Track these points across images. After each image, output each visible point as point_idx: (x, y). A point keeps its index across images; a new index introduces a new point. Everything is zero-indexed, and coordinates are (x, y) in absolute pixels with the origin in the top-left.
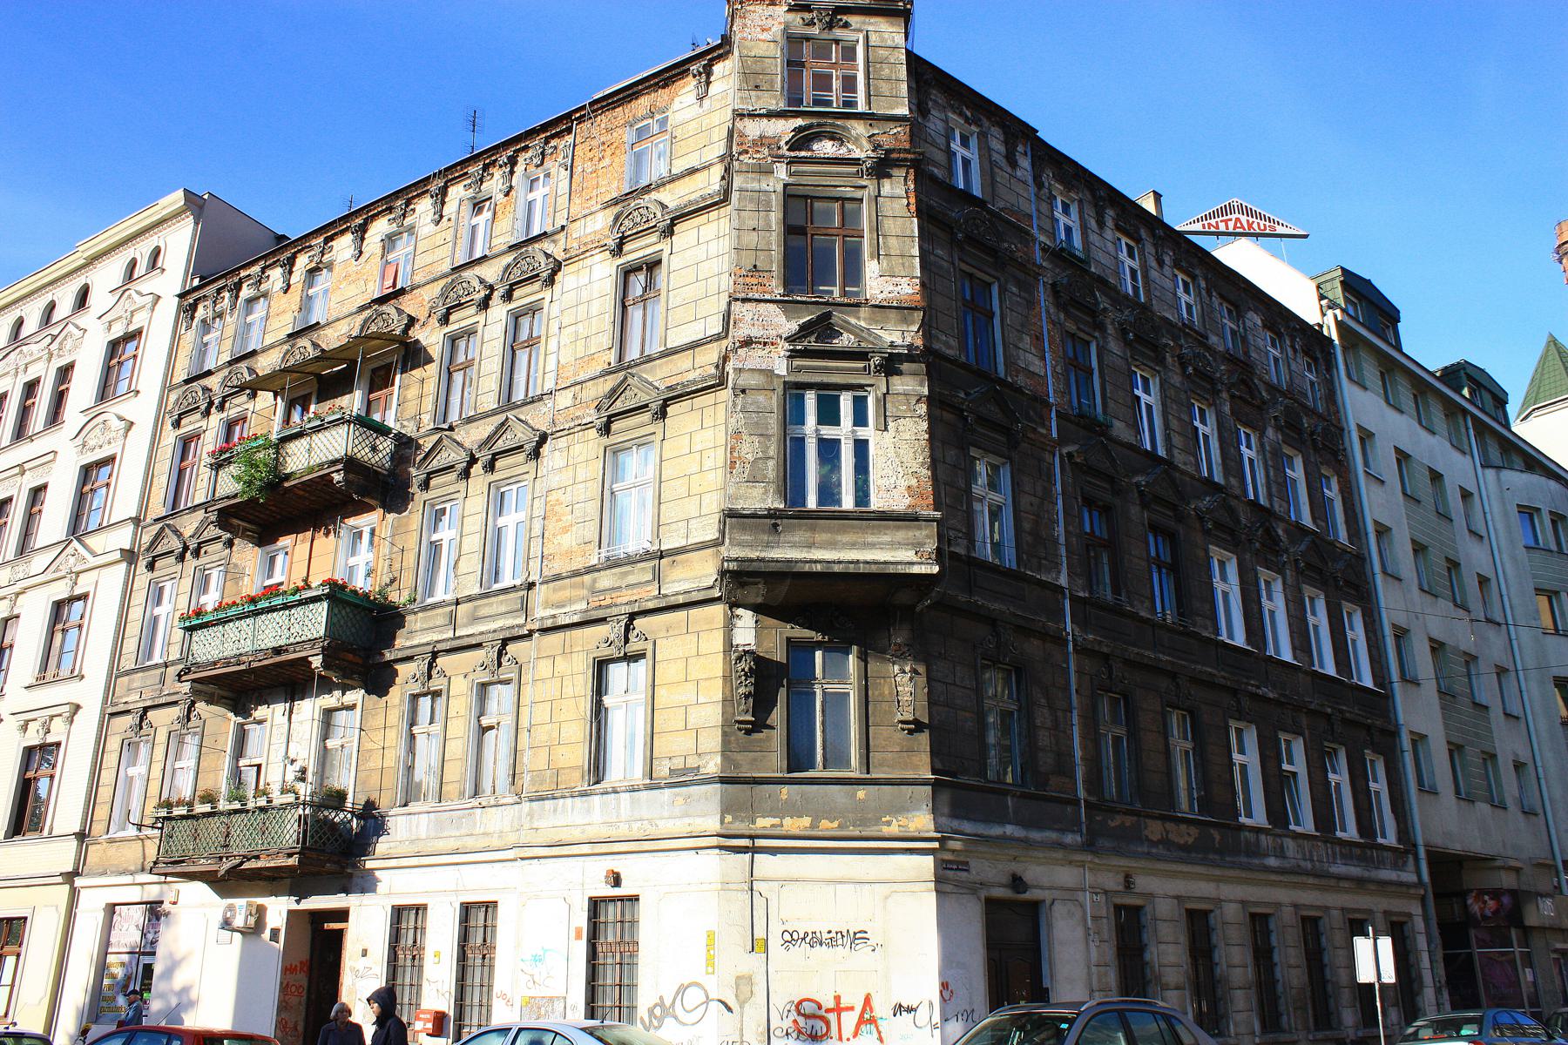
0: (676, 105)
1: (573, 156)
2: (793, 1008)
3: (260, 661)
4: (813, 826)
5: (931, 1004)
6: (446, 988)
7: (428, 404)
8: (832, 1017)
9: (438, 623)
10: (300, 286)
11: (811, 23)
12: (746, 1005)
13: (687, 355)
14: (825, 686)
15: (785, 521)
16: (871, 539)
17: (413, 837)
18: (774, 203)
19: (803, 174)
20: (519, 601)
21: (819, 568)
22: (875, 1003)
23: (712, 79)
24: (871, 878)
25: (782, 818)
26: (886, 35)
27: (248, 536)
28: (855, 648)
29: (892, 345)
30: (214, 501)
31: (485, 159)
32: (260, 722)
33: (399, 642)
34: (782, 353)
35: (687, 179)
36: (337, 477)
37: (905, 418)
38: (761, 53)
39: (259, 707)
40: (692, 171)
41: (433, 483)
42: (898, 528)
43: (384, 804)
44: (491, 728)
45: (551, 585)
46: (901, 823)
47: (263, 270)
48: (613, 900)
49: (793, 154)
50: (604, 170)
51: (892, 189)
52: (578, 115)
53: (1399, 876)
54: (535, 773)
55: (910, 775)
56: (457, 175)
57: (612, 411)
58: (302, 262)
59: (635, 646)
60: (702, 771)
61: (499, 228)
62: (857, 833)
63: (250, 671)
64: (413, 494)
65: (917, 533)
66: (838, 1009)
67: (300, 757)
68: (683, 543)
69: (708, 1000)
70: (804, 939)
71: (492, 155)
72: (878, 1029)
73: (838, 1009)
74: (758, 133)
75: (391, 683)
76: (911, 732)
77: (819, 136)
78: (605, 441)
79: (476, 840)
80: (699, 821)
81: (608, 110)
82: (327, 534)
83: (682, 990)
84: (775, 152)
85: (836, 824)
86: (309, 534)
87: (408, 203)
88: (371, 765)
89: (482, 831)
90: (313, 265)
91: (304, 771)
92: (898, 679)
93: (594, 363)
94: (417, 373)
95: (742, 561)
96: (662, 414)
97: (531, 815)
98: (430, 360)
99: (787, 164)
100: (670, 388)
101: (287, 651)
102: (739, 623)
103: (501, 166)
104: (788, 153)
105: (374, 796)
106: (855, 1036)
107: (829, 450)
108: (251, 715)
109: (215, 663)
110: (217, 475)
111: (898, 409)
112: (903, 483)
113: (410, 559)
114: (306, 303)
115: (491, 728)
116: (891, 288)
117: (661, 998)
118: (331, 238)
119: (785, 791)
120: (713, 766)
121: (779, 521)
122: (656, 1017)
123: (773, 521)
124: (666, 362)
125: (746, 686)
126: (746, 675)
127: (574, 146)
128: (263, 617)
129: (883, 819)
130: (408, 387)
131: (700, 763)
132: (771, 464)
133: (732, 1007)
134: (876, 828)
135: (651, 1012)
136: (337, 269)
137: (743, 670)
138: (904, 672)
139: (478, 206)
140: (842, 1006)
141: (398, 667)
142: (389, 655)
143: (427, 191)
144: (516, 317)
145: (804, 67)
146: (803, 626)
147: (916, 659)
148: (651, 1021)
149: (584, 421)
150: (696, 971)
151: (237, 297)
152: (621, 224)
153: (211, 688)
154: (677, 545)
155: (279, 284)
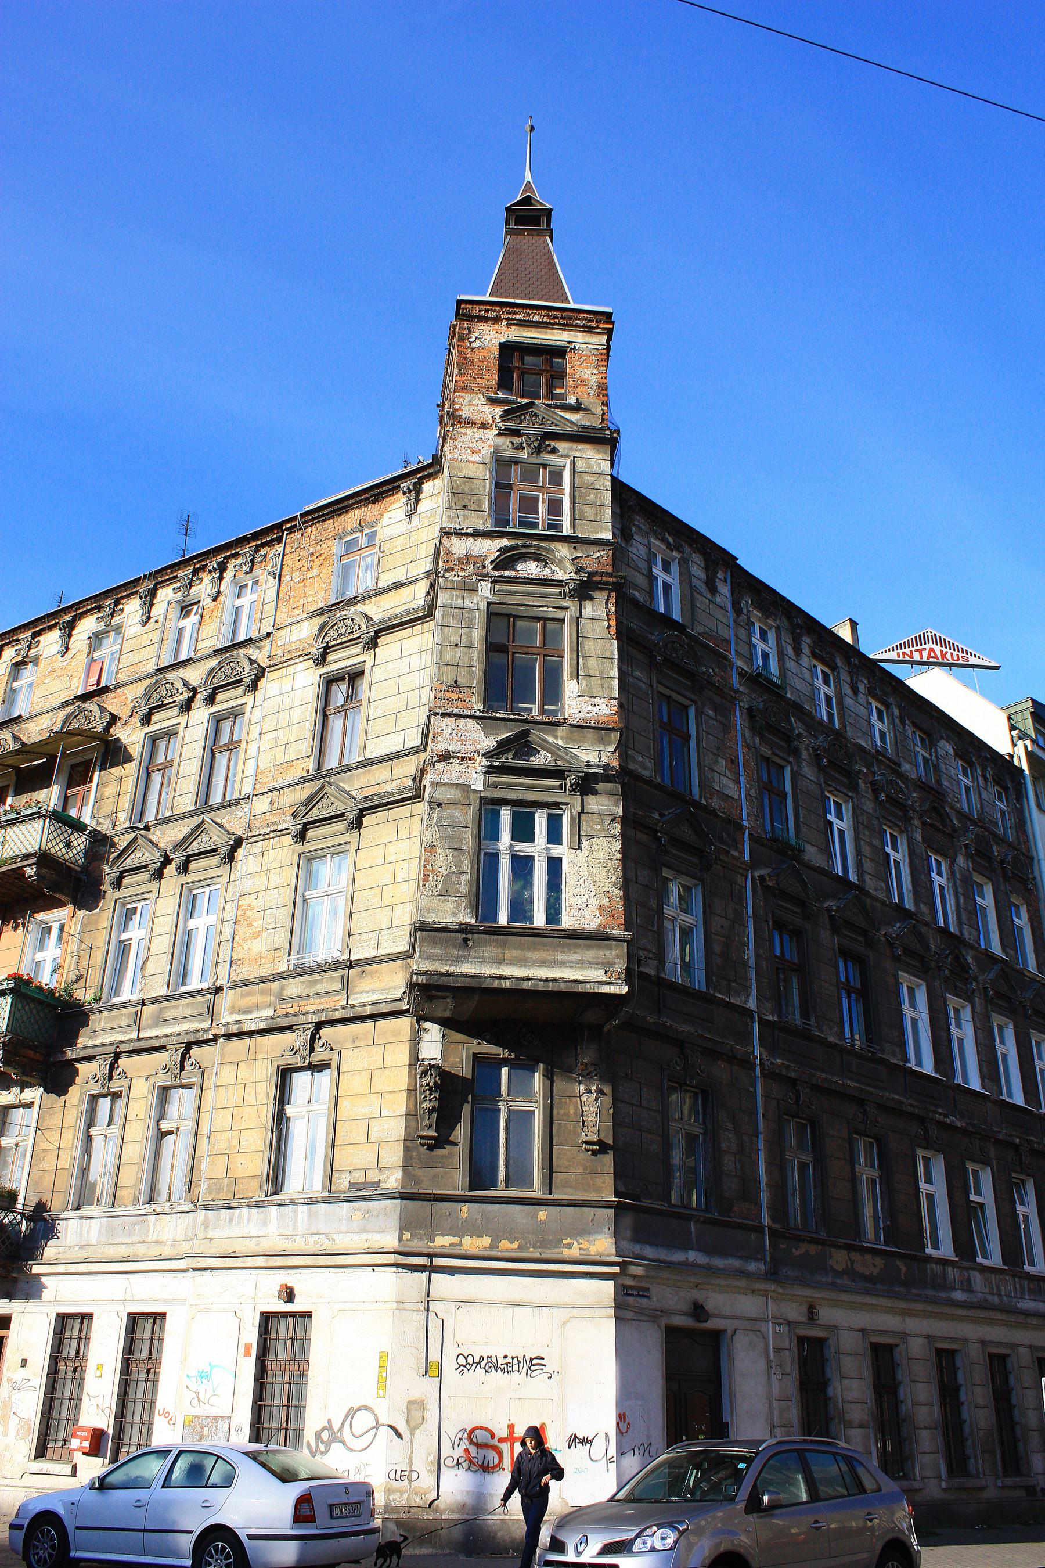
0: (385, 520)
2: (465, 1436)
4: (493, 1246)
5: (607, 1436)
9: (122, 1023)
11: (520, 447)
12: (417, 1432)
13: (385, 766)
14: (510, 1103)
15: (476, 936)
16: (561, 957)
17: (83, 1243)
21: (508, 984)
25: (462, 1237)
26: (593, 462)
31: (195, 564)
33: (82, 1041)
34: (480, 769)
35: (393, 593)
36: (29, 871)
37: (599, 837)
38: (470, 474)
40: (398, 586)
42: (589, 947)
43: (55, 1205)
44: (170, 1132)
45: (239, 990)
46: (581, 1246)
48: (285, 1315)
49: (497, 573)
51: (594, 611)
52: (288, 525)
55: (592, 1197)
59: (320, 1055)
60: (383, 1185)
65: (607, 953)
68: (373, 954)
69: (378, 1425)
70: (479, 1363)
71: (202, 560)
75: (71, 1082)
76: (595, 1153)
77: (523, 557)
78: (300, 848)
81: (318, 522)
83: (351, 1413)
85: (515, 1245)
89: (155, 1238)
90: (19, 658)
92: (584, 1099)
94: (116, 771)
95: (431, 975)
96: (357, 824)
97: (206, 1224)
98: (129, 759)
99: (491, 583)
102: (426, 1037)
104: (492, 572)
105: (46, 1198)
111: (592, 828)
112: (595, 902)
113: (98, 957)
115: (170, 1132)
116: (590, 708)
117: (329, 1421)
118: (39, 634)
120: (393, 1181)
121: (469, 936)
122: (323, 1442)
123: (464, 936)
125: (430, 1100)
126: (430, 1089)
127: (284, 555)
129: (565, 1242)
130: (105, 785)
131: (381, 1178)
132: (464, 878)
133: (402, 1433)
134: (556, 1250)
135: (318, 1435)
137: (428, 1084)
138: (590, 1092)
139: (185, 609)
140: (515, 1435)
143: (136, 592)
144: (218, 721)
146: (490, 1042)
148: (317, 1446)
154: (367, 956)
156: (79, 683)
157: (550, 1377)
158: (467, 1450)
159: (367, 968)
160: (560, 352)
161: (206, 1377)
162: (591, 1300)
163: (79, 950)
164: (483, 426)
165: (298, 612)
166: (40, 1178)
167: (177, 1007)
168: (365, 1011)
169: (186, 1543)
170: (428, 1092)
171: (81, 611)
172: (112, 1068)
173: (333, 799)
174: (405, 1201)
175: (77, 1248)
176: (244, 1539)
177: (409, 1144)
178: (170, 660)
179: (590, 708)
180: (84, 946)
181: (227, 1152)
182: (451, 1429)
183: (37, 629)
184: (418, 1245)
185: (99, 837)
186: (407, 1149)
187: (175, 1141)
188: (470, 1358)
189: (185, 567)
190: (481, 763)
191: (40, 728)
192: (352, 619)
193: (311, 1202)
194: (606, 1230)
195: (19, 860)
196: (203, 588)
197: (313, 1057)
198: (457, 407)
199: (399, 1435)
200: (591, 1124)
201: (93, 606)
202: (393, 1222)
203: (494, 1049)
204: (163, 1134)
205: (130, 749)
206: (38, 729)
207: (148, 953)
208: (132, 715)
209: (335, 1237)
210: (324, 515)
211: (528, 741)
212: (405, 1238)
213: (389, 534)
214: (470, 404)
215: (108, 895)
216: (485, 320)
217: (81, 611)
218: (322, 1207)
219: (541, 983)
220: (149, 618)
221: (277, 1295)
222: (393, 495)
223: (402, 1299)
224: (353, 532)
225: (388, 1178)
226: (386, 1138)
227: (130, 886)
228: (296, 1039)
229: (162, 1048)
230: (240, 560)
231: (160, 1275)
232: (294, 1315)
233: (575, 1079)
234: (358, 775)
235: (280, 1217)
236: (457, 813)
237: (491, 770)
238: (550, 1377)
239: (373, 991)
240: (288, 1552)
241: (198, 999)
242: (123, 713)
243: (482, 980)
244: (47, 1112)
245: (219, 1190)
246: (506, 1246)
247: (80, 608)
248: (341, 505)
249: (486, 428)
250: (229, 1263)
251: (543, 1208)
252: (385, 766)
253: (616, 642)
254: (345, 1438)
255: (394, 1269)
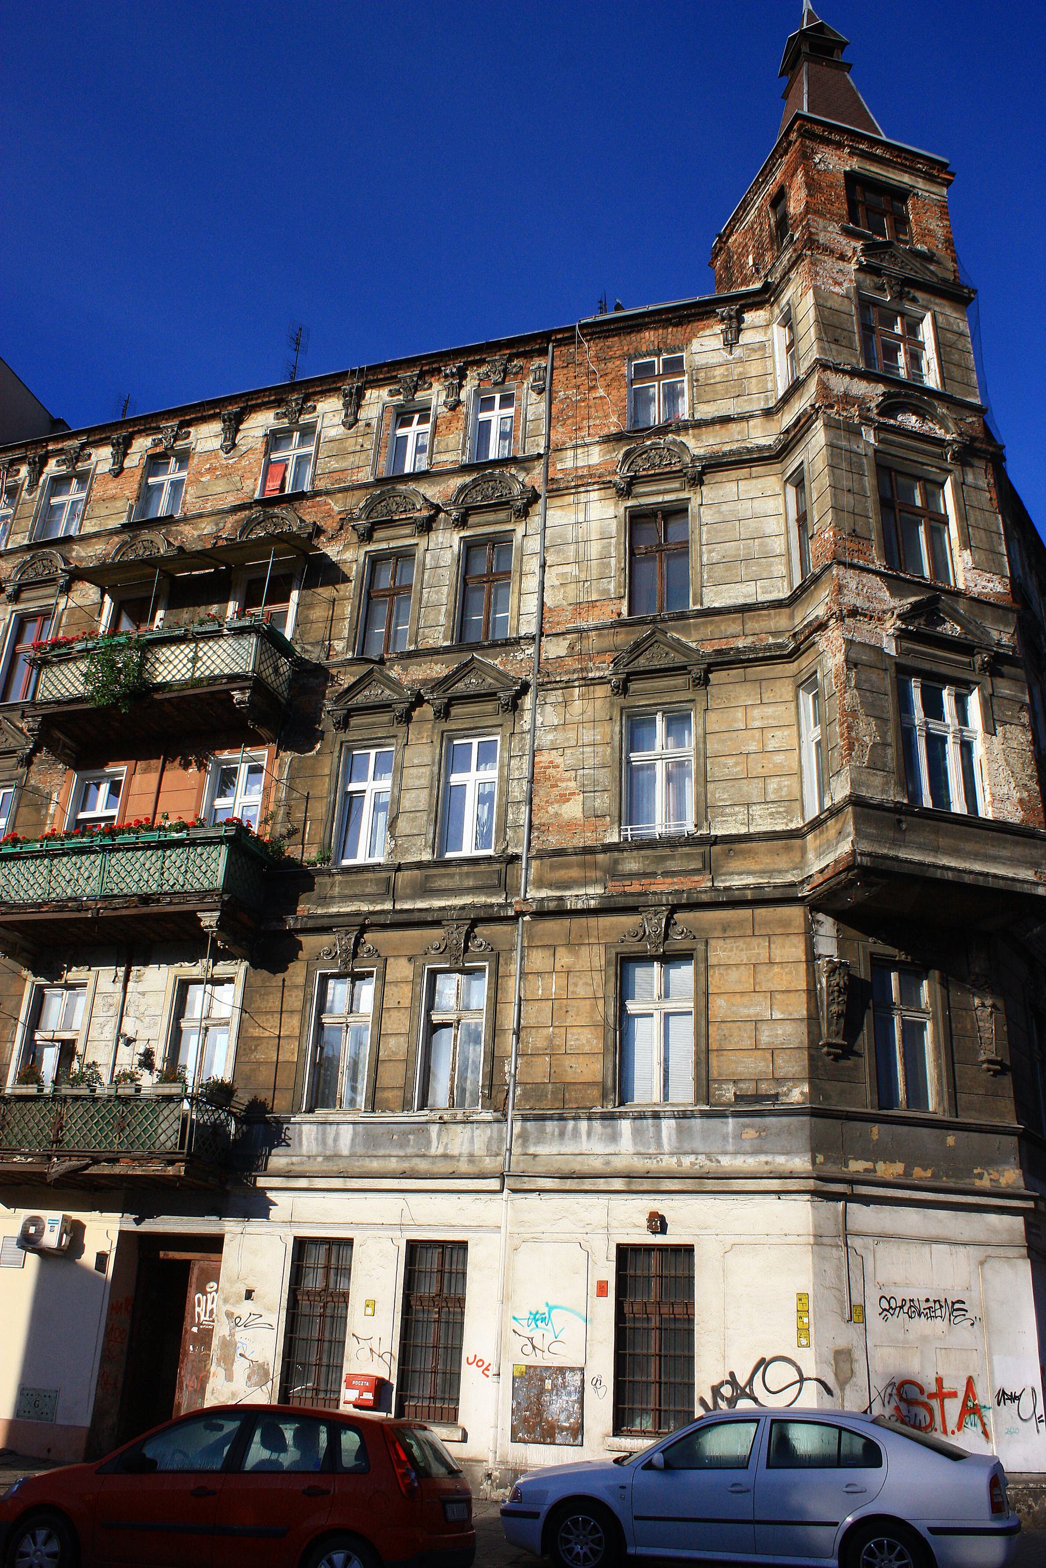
0: (695, 345)
1: (551, 379)
2: (895, 1391)
3: (116, 909)
4: (907, 1173)
5: (1033, 1390)
6: (386, 1347)
7: (344, 629)
8: (935, 1404)
9: (368, 890)
10: (138, 472)
11: (881, 289)
12: (847, 1387)
13: (735, 618)
14: (905, 1013)
15: (909, 818)
16: (992, 851)
17: (328, 1153)
18: (866, 468)
19: (891, 443)
20: (496, 876)
21: (950, 875)
22: (979, 1389)
23: (363, 403)
24: (965, 1238)
25: (875, 1162)
26: (952, 320)
27: (66, 755)
28: (936, 974)
29: (999, 644)
30: (33, 703)
31: (423, 365)
32: (69, 987)
33: (302, 908)
34: (891, 631)
35: (717, 427)
36: (237, 695)
37: (1011, 724)
38: (836, 306)
39: (74, 969)
40: (725, 420)
41: (354, 721)
42: (1017, 843)
43: (280, 1105)
44: (447, 1025)
45: (548, 861)
46: (992, 1177)
47: (83, 447)
48: (649, 1249)
49: (882, 420)
50: (597, 401)
51: (975, 479)
52: (559, 336)
53: (658, 1223)
54: (528, 1086)
55: (996, 1122)
56: (382, 376)
57: (631, 668)
58: (142, 445)
59: (678, 942)
60: (784, 1099)
61: (443, 444)
62: (951, 1184)
63: (96, 921)
64: (323, 732)
65: (1034, 852)
66: (941, 1395)
67: (143, 1035)
68: (743, 830)
69: (802, 1380)
70: (901, 1307)
71: (434, 363)
72: (982, 1421)
73: (941, 1395)
74: (842, 389)
75: (293, 957)
76: (996, 1073)
77: (905, 408)
78: (620, 701)
79: (433, 1163)
80: (781, 1160)
81: (599, 338)
82: (186, 766)
83: (763, 1364)
84: (864, 413)
85: (929, 1173)
86: (157, 763)
87: (306, 399)
88: (260, 1056)
89: (440, 1151)
90: (158, 450)
91: (148, 1054)
92: (979, 1013)
93: (596, 612)
94: (325, 592)
95: (876, 857)
96: (704, 682)
97: (524, 1136)
98: (346, 579)
99: (875, 429)
100: (719, 652)
101: (158, 901)
102: (822, 931)
103: (446, 376)
104: (877, 418)
105: (264, 1096)
106: (959, 1429)
107: (936, 744)
108: (61, 977)
109: (40, 905)
110: (38, 675)
111: (1004, 714)
112: (1016, 795)
113: (319, 809)
114: (147, 494)
115: (447, 1025)
116: (984, 583)
117: (732, 1374)
118: (189, 424)
119: (875, 1131)
120: (797, 1094)
121: (903, 818)
122: (723, 1397)
123: (898, 817)
124: (703, 623)
125: (838, 1003)
126: (839, 991)
127: (553, 369)
128: (120, 855)
129: (975, 1171)
130: (310, 606)
131: (780, 1090)
132: (890, 752)
133: (832, 1388)
134: (967, 1181)
135: (716, 1391)
136: (194, 462)
137: (838, 985)
138: (983, 1005)
139: (403, 417)
140: (945, 1390)
141: (304, 939)
142: (291, 923)
143: (339, 389)
144: (470, 547)
145: (874, 332)
146: (886, 942)
147: (993, 993)
148: (715, 1403)
149: (591, 675)
150: (785, 1342)
151: (41, 473)
152: (632, 462)
153: (14, 936)
154: (734, 832)
155: (105, 467)
156: (255, 485)
157: (972, 1324)
158: (897, 1408)
159: (737, 846)
160: (902, 194)
161: (543, 1320)
162: (1004, 1238)
163: (288, 798)
164: (842, 257)
165: (583, 434)
166: (252, 1070)
167: (452, 876)
168: (744, 895)
169: (828, 1538)
170: (836, 994)
171: (254, 402)
172: (357, 943)
173: (667, 649)
174: (814, 1119)
175: (320, 1159)
176: (926, 1534)
177: (813, 1052)
178: (388, 471)
179: (984, 583)
180: (295, 795)
181: (548, 1052)
182: (879, 1384)
183: (187, 418)
184: (832, 1170)
185: (308, 667)
186: (811, 1058)
187: (456, 1036)
188: (892, 1301)
189: (409, 367)
190: (891, 625)
191: (199, 532)
192: (669, 450)
193: (683, 1115)
194: (1012, 1160)
195: (224, 681)
196: (436, 394)
197: (669, 945)
198: (813, 230)
199: (829, 1391)
200: (988, 1041)
201: (273, 398)
202: (802, 1139)
203: (890, 950)
204: (433, 1028)
205: (345, 569)
206: (196, 533)
207: (398, 809)
208: (341, 528)
209: (720, 1158)
210: (608, 331)
211: (937, 608)
212: (818, 1162)
213: (703, 362)
214: (825, 229)
215: (329, 736)
216: (827, 142)
217: (254, 402)
218: (697, 1123)
219: (981, 878)
220: (357, 421)
221: (645, 1224)
222: (702, 320)
223: (820, 1231)
224: (649, 354)
225: (790, 1090)
226: (783, 1044)
227: (359, 727)
228: (653, 923)
229: (436, 923)
230: (484, 369)
231: (455, 1196)
232: (662, 1248)
233: (969, 991)
234: (696, 625)
235: (637, 1133)
236: (874, 677)
237: (902, 635)
238: (972, 1324)
239: (749, 873)
240: (993, 1549)
241: (482, 868)
242: (330, 525)
243: (925, 868)
244: (257, 992)
245: (541, 1097)
246: (919, 1173)
247: (252, 399)
248: (634, 322)
249: (844, 261)
250: (569, 1184)
251: (951, 1132)
252: (735, 618)
253: (1000, 517)
254: (756, 1394)
255: (808, 1197)
